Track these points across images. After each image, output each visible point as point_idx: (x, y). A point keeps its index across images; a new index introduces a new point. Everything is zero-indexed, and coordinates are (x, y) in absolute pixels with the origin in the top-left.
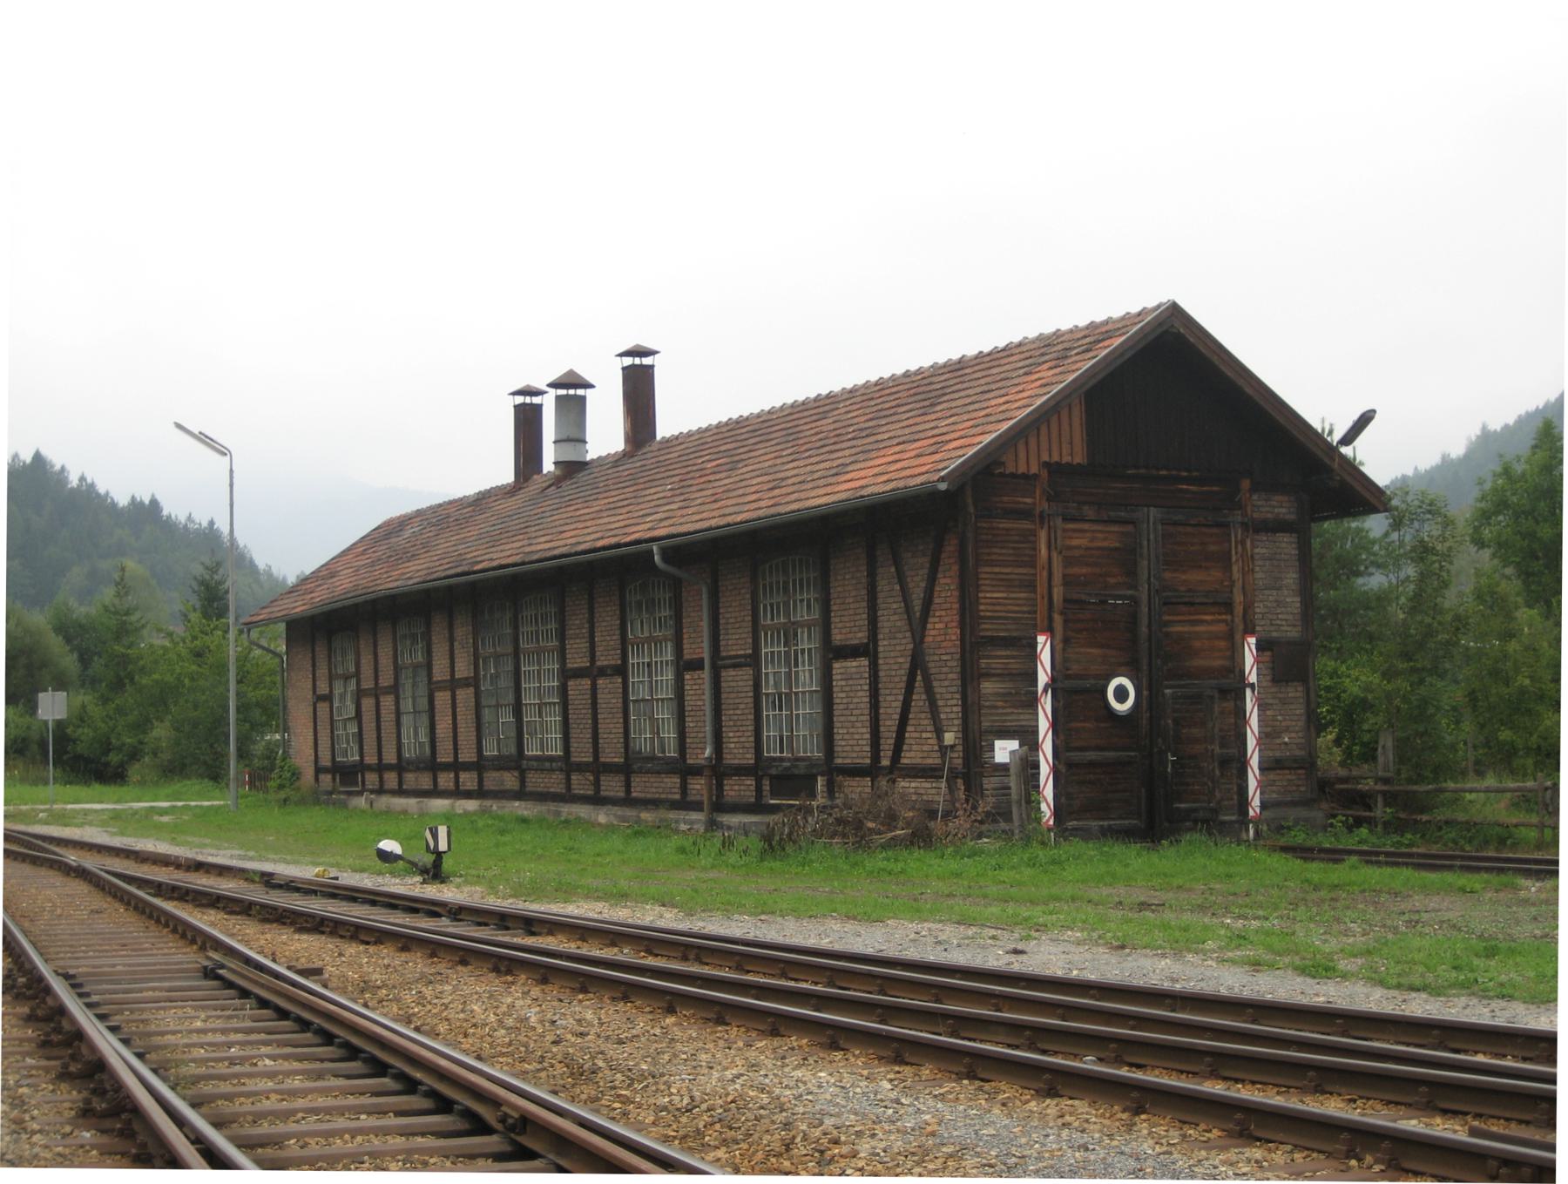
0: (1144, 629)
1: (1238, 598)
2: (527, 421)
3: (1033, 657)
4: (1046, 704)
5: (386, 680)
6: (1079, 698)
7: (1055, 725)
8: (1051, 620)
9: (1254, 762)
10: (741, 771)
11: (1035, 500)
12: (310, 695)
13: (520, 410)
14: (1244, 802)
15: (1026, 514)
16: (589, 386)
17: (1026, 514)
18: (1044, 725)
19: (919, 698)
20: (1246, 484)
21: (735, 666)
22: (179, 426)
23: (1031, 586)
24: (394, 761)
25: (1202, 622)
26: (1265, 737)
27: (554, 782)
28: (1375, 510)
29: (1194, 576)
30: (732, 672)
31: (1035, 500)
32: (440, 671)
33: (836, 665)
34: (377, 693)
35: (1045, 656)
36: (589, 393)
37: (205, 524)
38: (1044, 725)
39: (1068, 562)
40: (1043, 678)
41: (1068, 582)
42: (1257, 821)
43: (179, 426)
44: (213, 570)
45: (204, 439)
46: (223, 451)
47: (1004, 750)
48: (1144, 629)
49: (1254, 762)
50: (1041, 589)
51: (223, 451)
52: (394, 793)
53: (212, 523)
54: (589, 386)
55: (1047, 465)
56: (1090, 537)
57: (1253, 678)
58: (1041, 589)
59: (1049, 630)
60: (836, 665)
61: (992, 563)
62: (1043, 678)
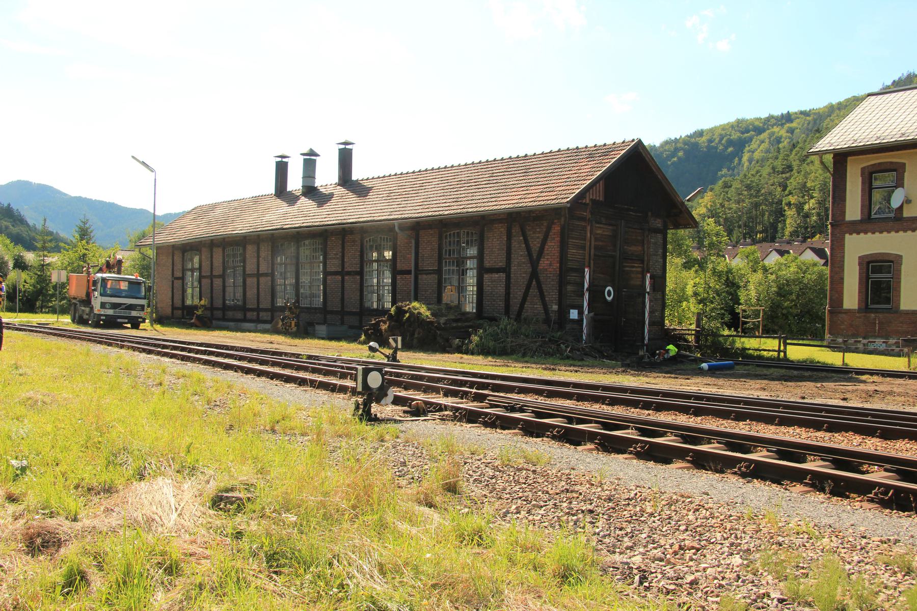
0: (617, 268)
1: (646, 258)
2: (282, 169)
3: (584, 277)
4: (587, 295)
5: (218, 271)
6: (596, 292)
7: (589, 305)
8: (590, 263)
9: (647, 322)
10: (266, 310)
11: (587, 214)
12: (170, 277)
13: (278, 164)
14: (644, 338)
15: (583, 219)
16: (317, 155)
17: (583, 219)
18: (586, 304)
19: (534, 291)
20: (650, 214)
21: (427, 274)
22: (133, 157)
23: (583, 248)
24: (221, 306)
25: (634, 267)
26: (651, 312)
27: (239, 315)
28: (685, 227)
29: (633, 248)
30: (425, 276)
31: (587, 214)
32: (251, 267)
33: (486, 276)
34: (258, 275)
35: (587, 277)
36: (317, 158)
37: (6, 205)
38: (586, 304)
39: (596, 239)
40: (586, 286)
41: (596, 248)
42: (646, 345)
43: (133, 157)
44: (85, 223)
45: (144, 163)
46: (152, 170)
47: (574, 314)
48: (617, 268)
49: (647, 322)
50: (587, 248)
51: (152, 170)
52: (219, 319)
53: (9, 205)
54: (317, 155)
55: (591, 200)
56: (602, 230)
57: (648, 290)
58: (587, 248)
59: (589, 267)
60: (486, 276)
61: (573, 238)
62: (586, 286)
